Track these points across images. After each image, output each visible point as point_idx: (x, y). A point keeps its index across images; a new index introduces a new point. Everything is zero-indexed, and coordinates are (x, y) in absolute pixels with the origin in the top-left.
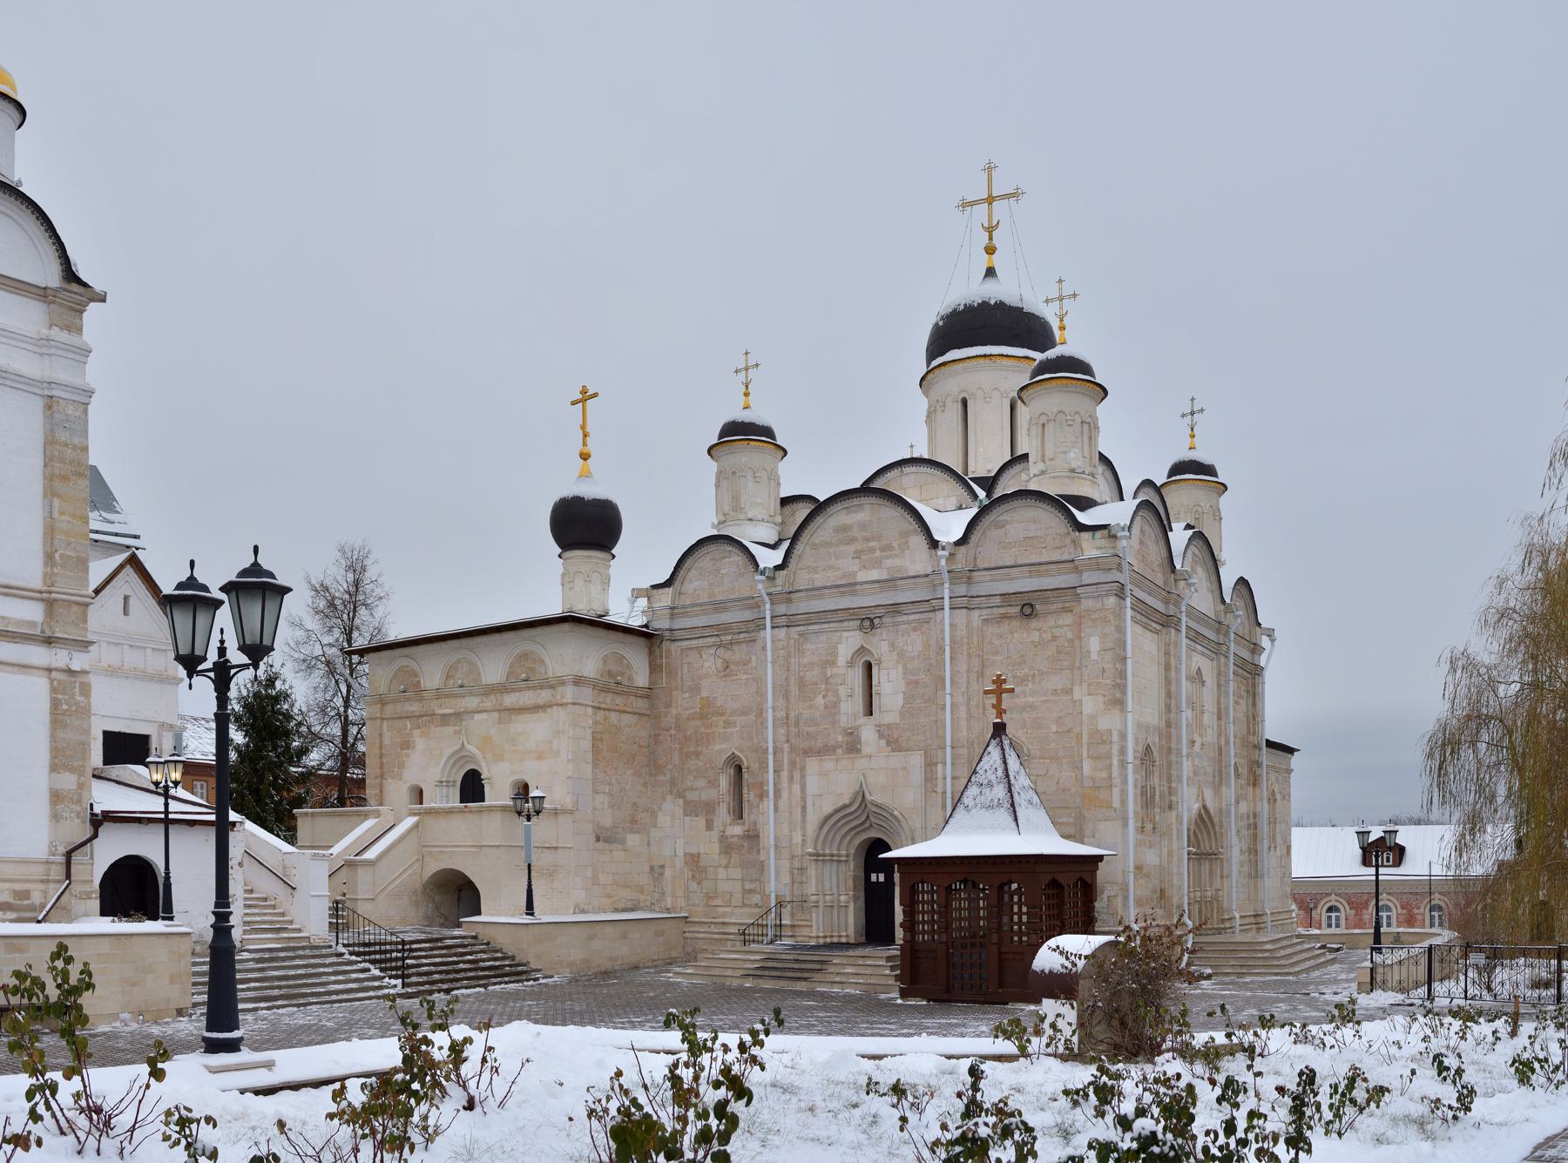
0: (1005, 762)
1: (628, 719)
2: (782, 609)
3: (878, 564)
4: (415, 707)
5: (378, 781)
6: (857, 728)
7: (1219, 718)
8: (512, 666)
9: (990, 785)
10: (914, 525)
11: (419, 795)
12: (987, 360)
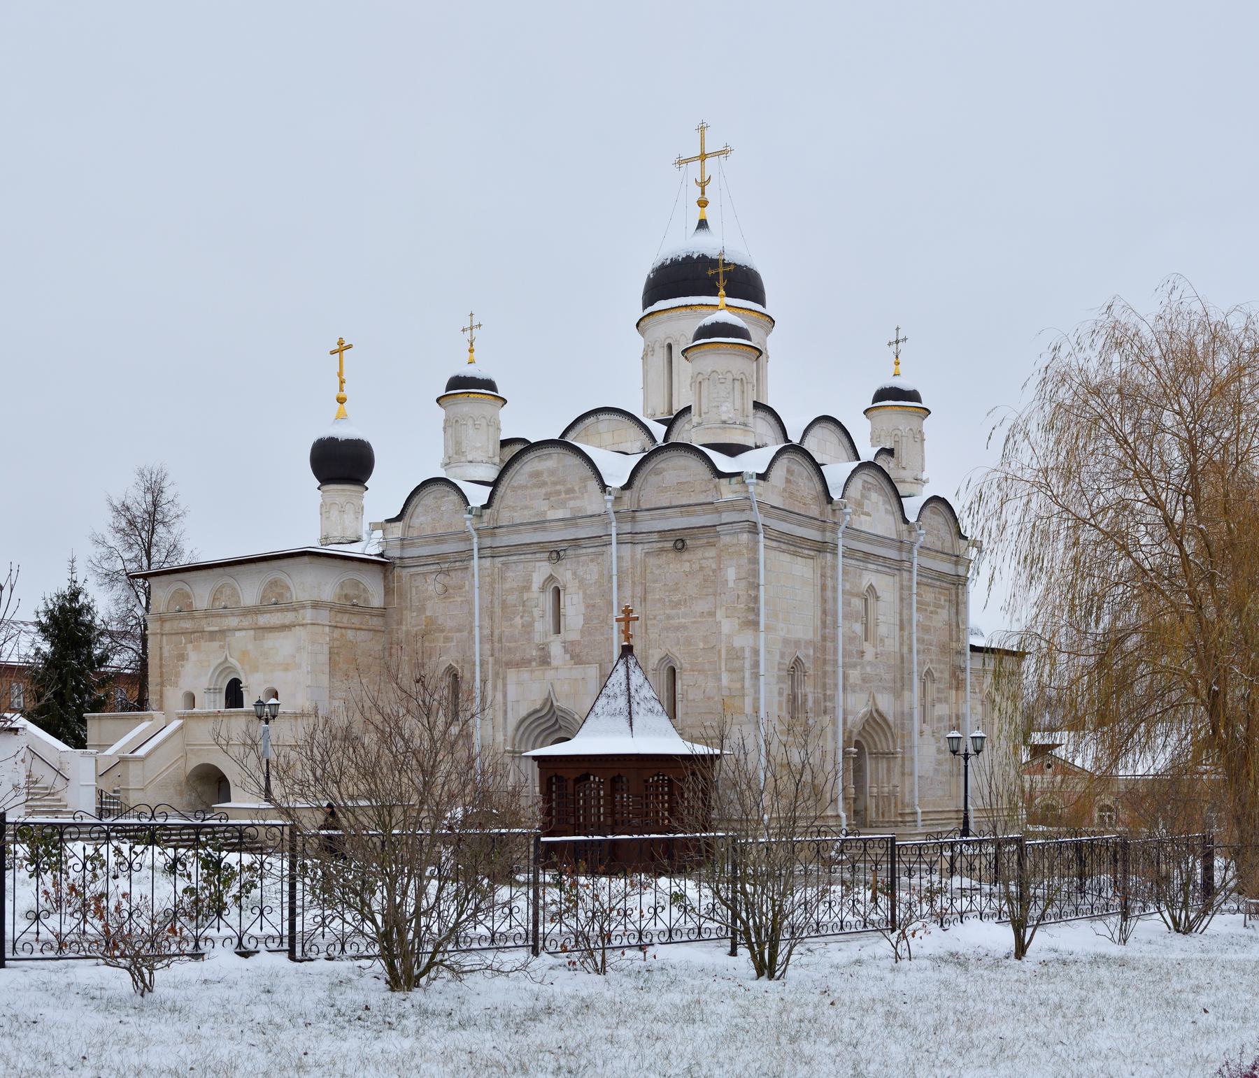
0: (628, 678)
1: (362, 635)
2: (487, 542)
3: (563, 504)
4: (187, 625)
5: (158, 688)
6: (547, 644)
7: (902, 628)
8: (265, 590)
9: (615, 697)
10: (590, 473)
11: (191, 699)
12: (688, 310)
